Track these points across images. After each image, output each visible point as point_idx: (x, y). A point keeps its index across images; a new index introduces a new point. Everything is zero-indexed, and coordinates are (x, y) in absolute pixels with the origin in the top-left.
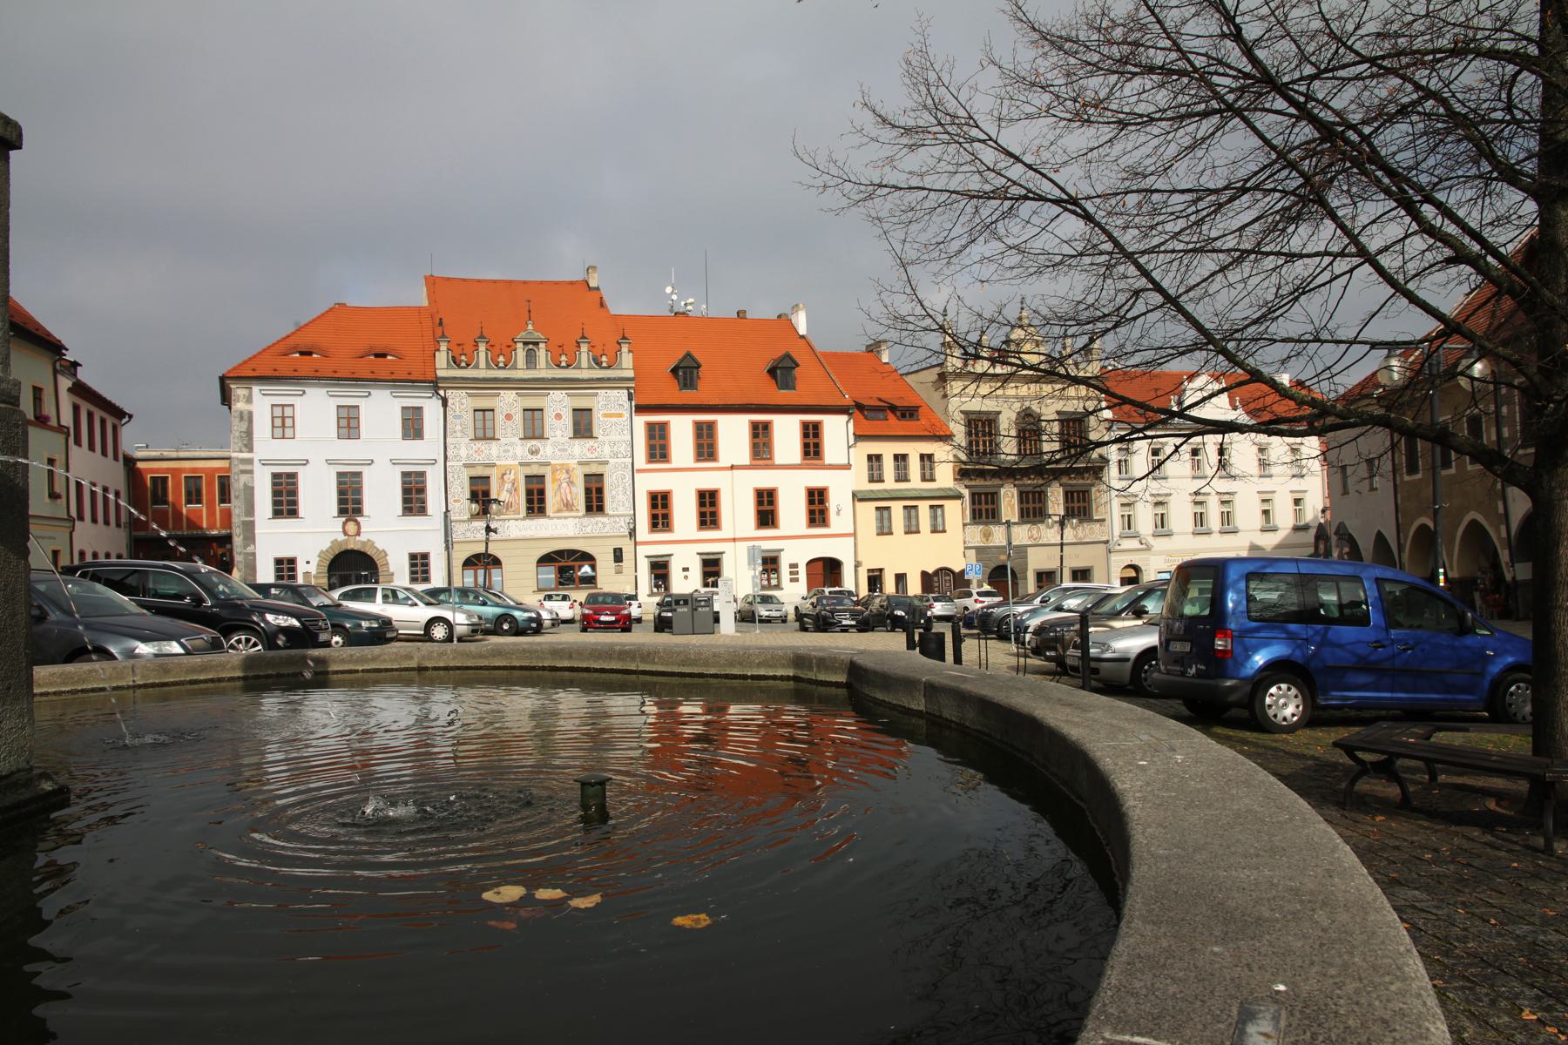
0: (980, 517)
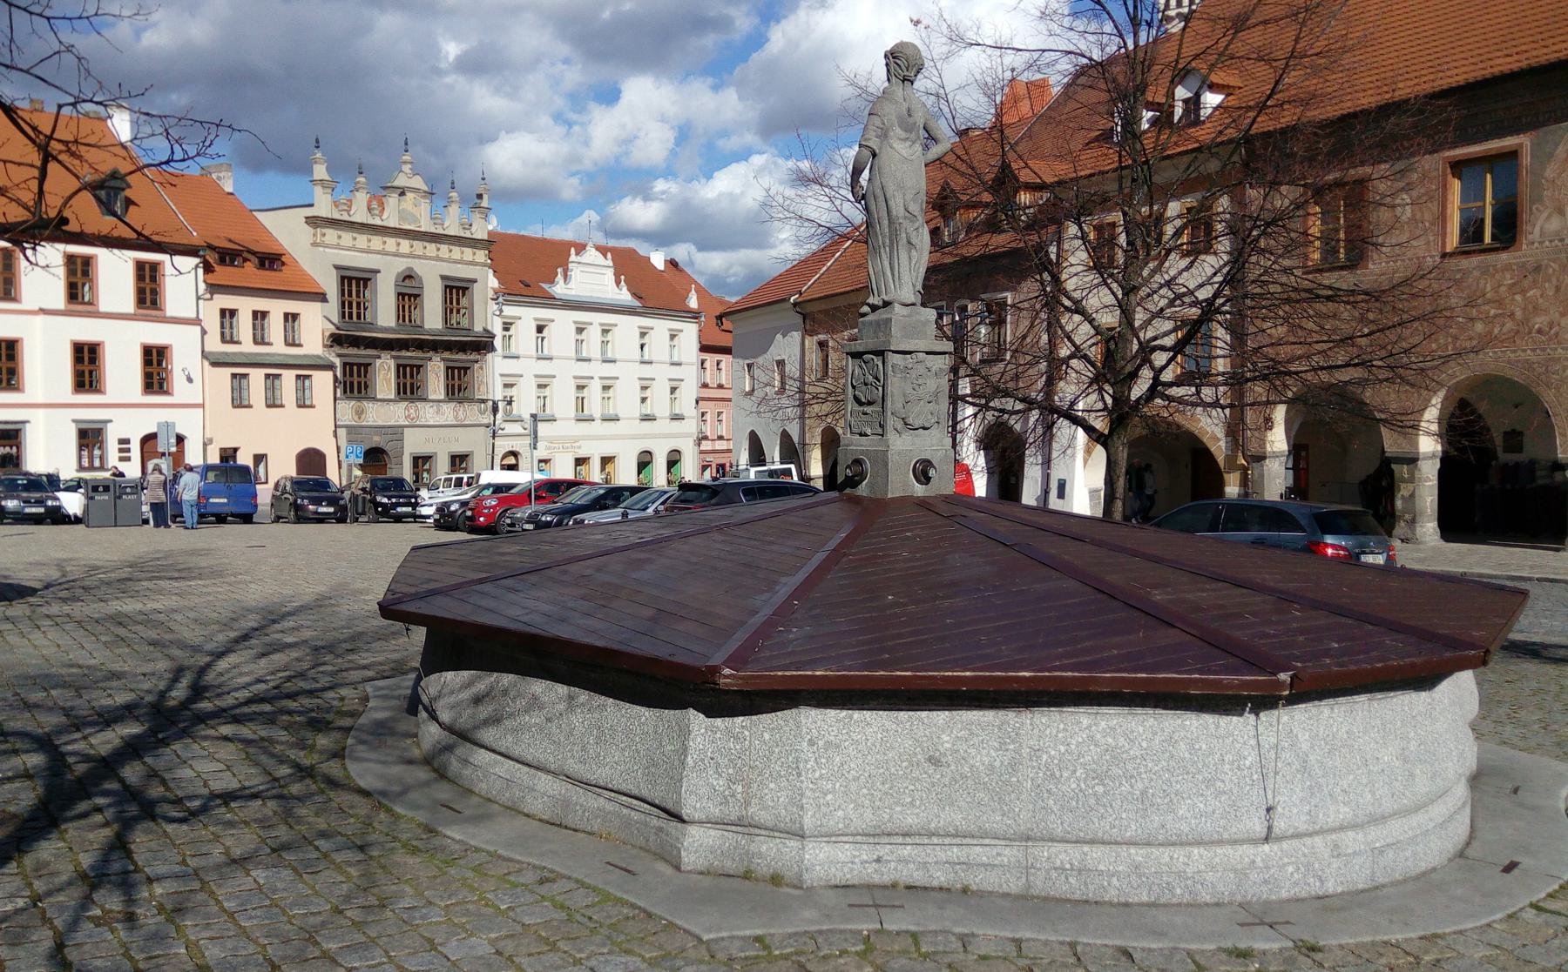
0: (352, 391)
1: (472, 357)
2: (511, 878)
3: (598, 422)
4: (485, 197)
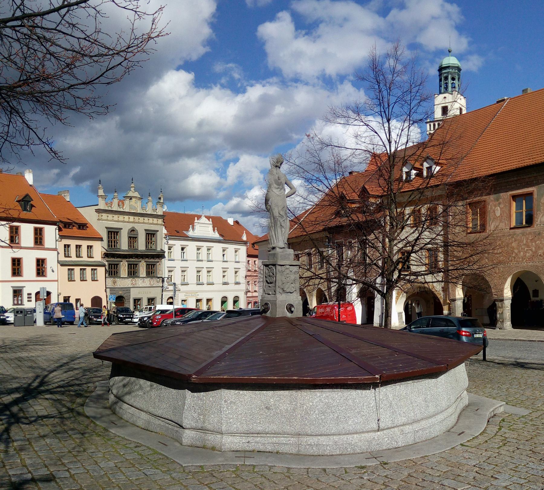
0: (112, 275)
1: (156, 260)
2: (127, 445)
3: (205, 285)
4: (162, 199)
